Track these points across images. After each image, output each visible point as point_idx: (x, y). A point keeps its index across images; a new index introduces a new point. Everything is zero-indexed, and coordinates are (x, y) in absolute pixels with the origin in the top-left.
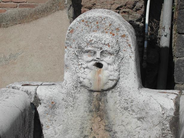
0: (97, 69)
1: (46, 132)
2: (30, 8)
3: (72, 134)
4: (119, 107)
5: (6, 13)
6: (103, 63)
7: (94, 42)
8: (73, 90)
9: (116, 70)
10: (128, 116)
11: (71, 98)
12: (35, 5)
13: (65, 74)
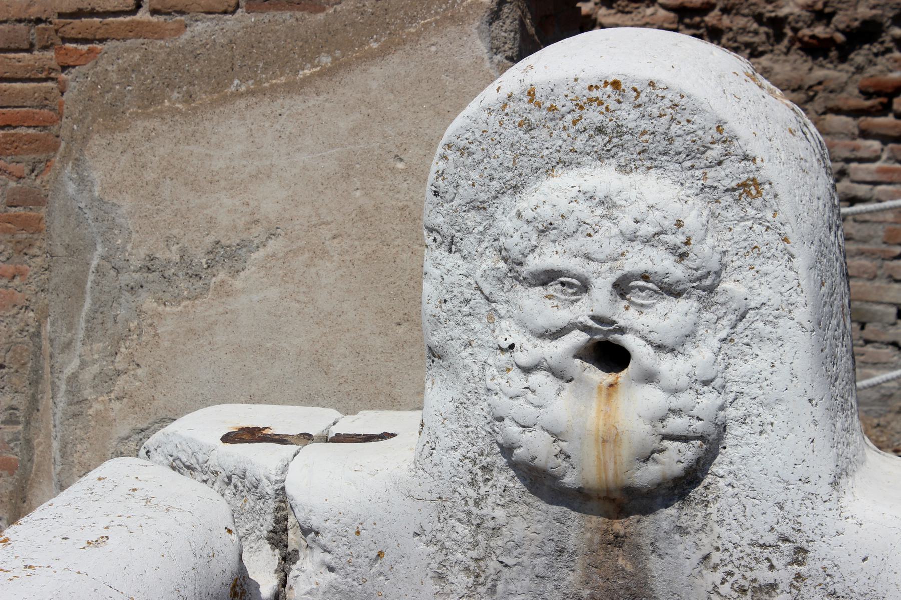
0: (597, 376)
2: (299, 14)
4: (727, 586)
5: (186, 36)
6: (629, 341)
7: (575, 224)
8: (473, 483)
9: (706, 383)
11: (459, 527)
13: (428, 391)
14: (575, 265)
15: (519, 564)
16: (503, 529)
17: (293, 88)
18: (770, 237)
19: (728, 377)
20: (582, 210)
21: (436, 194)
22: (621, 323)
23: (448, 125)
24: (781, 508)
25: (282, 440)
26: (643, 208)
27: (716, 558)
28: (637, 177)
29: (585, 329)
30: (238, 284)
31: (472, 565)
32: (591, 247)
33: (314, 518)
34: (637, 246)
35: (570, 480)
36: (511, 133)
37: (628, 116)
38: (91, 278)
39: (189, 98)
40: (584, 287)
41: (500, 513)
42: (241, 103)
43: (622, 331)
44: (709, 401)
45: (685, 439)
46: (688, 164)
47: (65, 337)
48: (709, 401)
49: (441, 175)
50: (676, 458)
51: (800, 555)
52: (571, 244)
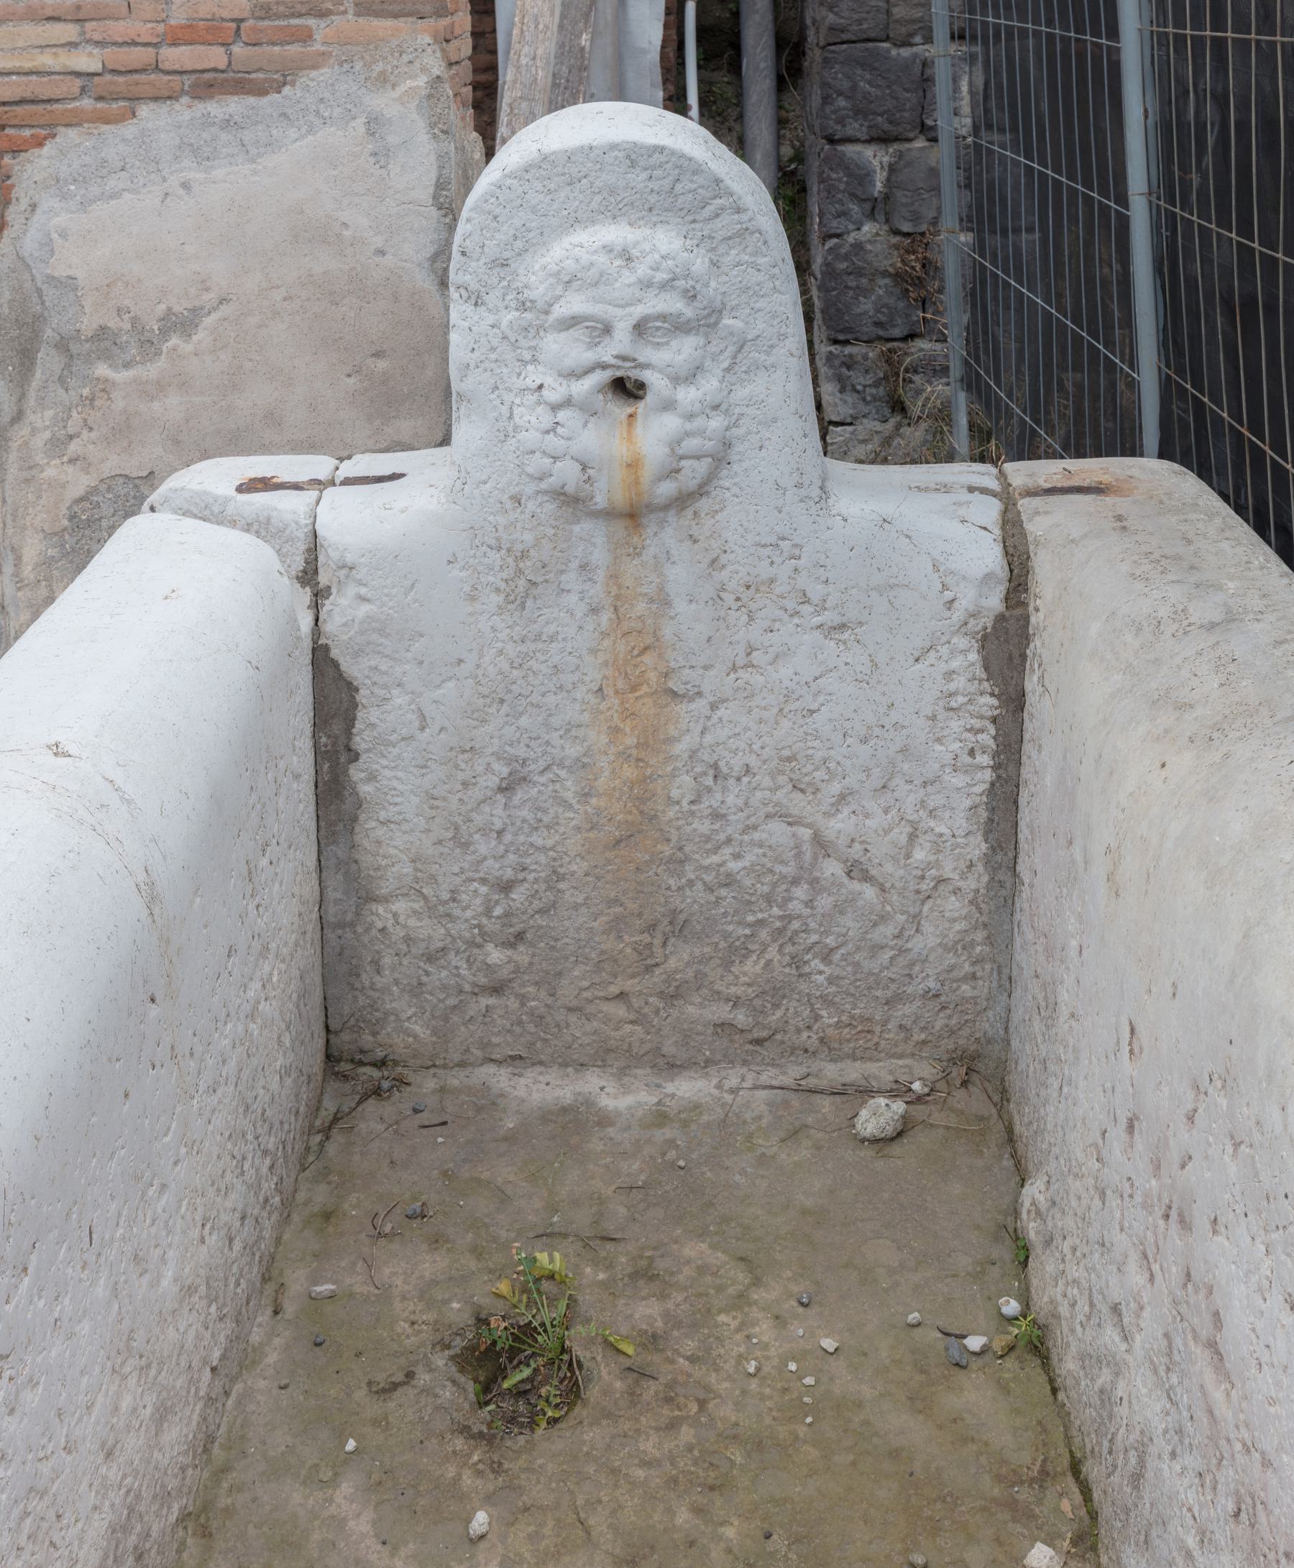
0: (620, 410)
1: (373, 720)
3: (507, 723)
6: (647, 376)
10: (781, 620)
11: (491, 554)
12: (529, 1379)
15: (546, 581)
16: (532, 551)
19: (732, 401)
21: (464, 254)
22: (642, 359)
24: (780, 512)
25: (296, 487)
26: (657, 256)
29: (604, 367)
31: (503, 585)
33: (349, 555)
34: (652, 292)
40: (607, 330)
43: (643, 366)
44: (716, 423)
46: (690, 218)
48: (716, 423)
50: (691, 475)
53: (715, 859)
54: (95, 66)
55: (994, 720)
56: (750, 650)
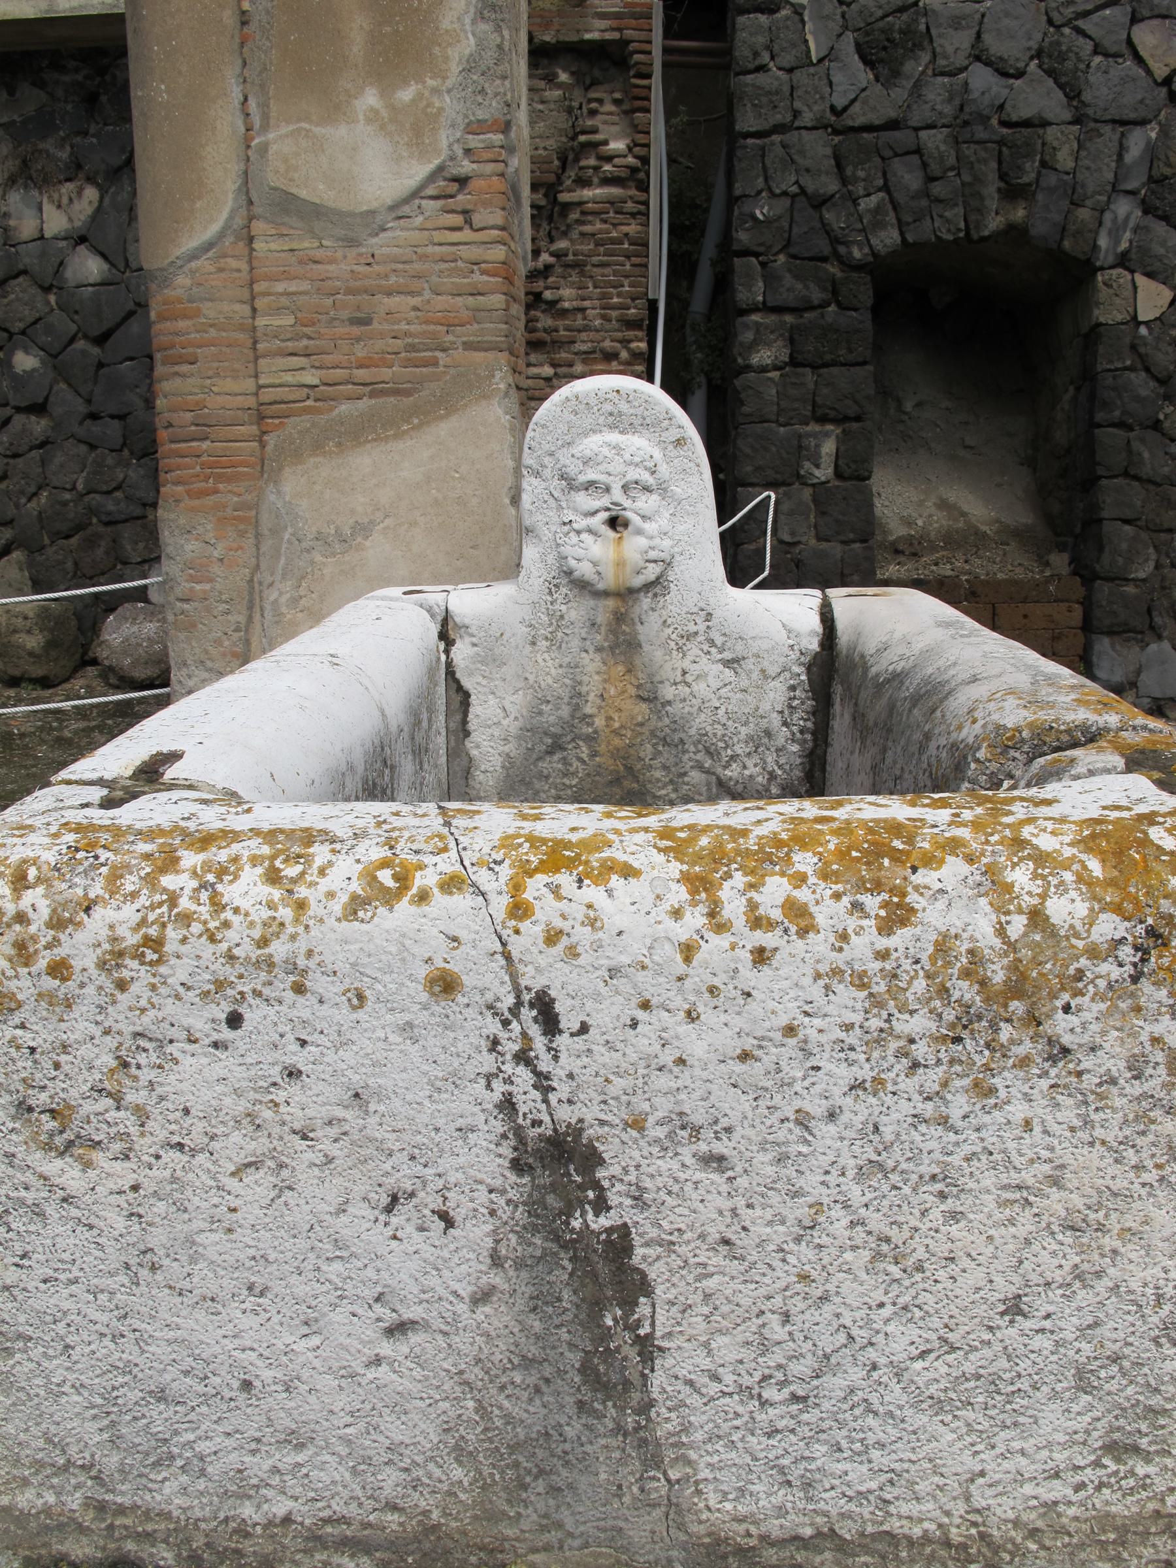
5: (337, 411)
6: (629, 514)
14: (602, 478)
17: (396, 437)
18: (691, 464)
20: (605, 451)
23: (592, 373)
27: (669, 621)
28: (629, 436)
29: (608, 509)
30: (368, 543)
32: (610, 468)
35: (601, 586)
36: (567, 416)
37: (624, 407)
38: (284, 546)
39: (339, 444)
41: (563, 608)
42: (369, 446)
45: (655, 561)
47: (270, 579)
49: (533, 439)
51: (709, 617)
52: (600, 468)
53: (663, 792)
54: (316, 381)
55: (814, 714)
56: (684, 673)
